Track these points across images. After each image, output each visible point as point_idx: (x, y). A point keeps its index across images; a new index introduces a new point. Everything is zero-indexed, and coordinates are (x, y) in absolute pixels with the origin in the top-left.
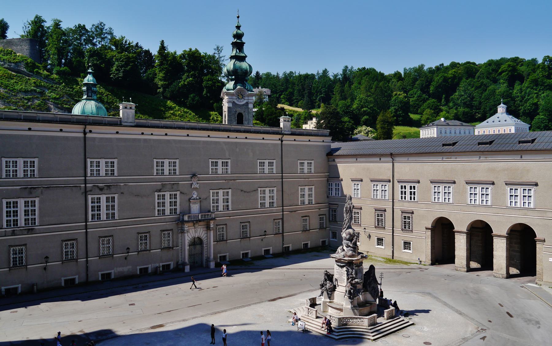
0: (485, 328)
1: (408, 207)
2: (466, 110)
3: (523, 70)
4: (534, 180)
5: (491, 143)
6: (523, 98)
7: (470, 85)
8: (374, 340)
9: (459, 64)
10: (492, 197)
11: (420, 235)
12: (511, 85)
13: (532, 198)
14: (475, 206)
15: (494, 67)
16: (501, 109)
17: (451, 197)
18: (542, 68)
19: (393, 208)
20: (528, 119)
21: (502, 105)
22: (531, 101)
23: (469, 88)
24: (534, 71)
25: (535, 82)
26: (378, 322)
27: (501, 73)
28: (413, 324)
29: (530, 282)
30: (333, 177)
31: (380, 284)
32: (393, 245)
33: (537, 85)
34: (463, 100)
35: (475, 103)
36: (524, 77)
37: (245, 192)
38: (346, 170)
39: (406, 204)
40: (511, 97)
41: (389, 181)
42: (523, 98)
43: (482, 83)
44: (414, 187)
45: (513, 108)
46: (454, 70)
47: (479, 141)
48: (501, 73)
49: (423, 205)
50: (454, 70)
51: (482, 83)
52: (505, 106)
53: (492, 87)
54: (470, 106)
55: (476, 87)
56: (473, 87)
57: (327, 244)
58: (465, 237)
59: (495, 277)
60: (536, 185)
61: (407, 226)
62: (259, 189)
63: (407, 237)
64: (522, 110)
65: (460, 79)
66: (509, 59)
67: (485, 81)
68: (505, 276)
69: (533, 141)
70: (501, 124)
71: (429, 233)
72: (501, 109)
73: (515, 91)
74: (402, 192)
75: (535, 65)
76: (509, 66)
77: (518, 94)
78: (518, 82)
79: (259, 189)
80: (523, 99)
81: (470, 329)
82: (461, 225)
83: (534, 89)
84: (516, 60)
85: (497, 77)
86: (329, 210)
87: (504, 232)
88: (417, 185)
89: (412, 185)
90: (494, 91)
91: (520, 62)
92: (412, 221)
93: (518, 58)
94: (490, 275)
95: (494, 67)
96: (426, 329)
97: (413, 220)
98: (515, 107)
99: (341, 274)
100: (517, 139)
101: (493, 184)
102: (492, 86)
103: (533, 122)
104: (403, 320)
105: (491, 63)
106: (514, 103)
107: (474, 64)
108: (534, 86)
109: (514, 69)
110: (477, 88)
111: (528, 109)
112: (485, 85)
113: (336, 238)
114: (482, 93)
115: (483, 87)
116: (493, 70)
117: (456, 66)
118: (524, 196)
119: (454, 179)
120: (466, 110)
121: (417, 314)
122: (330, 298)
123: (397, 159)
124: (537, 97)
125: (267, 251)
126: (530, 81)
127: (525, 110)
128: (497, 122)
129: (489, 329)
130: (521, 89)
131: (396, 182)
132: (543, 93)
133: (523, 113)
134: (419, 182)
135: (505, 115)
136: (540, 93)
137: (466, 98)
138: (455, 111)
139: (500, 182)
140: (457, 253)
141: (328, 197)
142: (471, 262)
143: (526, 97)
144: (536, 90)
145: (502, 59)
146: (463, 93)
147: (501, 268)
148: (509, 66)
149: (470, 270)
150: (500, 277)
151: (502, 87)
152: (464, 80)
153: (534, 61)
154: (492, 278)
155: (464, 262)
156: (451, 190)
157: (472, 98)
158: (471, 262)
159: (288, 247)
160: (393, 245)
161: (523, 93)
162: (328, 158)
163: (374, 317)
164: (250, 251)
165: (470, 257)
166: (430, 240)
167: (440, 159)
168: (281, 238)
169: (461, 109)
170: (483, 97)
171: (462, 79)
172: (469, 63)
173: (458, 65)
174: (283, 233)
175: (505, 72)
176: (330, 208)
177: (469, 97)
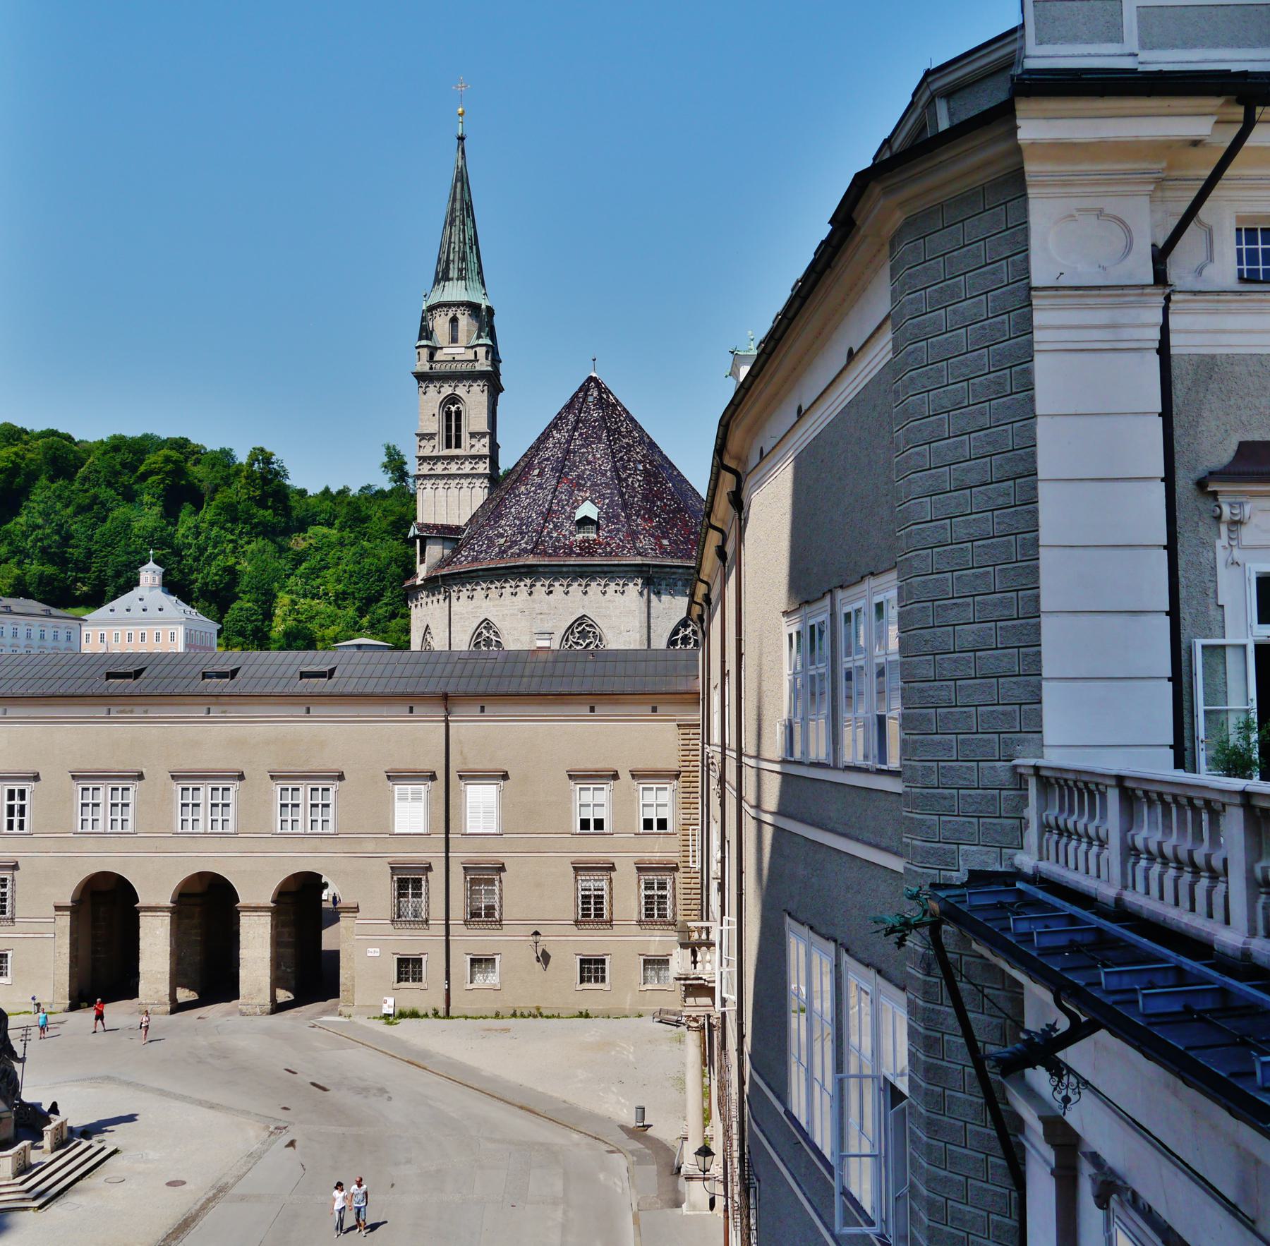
0: (282, 1124)
2: (49, 570)
3: (199, 476)
4: (335, 766)
5: (137, 674)
6: (201, 550)
7: (60, 497)
8: (40, 1207)
9: (24, 431)
11: (37, 928)
12: (171, 513)
13: (331, 809)
14: (193, 836)
15: (128, 457)
16: (150, 575)
17: (130, 817)
18: (247, 478)
20: (214, 607)
21: (151, 565)
22: (220, 561)
23: (59, 506)
24: (227, 481)
25: (231, 513)
26: (34, 1162)
27: (144, 477)
28: (115, 1152)
29: (325, 1012)
31: (22, 1060)
33: (234, 520)
34: (41, 540)
35: (75, 553)
36: (202, 496)
40: (170, 546)
42: (201, 550)
43: (95, 497)
44: (22, 794)
45: (176, 576)
46: (15, 449)
47: (105, 669)
48: (144, 477)
49: (49, 843)
50: (15, 449)
51: (95, 497)
52: (160, 570)
53: (121, 511)
54: (59, 559)
55: (79, 506)
56: (67, 506)
58: (167, 920)
59: (243, 1014)
60: (341, 777)
64: (198, 584)
65: (32, 477)
66: (165, 441)
67: (105, 493)
68: (268, 1007)
69: (233, 674)
70: (147, 621)
71: (65, 920)
72: (150, 575)
73: (181, 531)
74: (11, 808)
75: (228, 466)
76: (167, 460)
77: (190, 540)
78: (188, 507)
80: (202, 554)
81: (252, 1133)
82: (155, 889)
83: (226, 529)
84: (181, 444)
85: (136, 487)
87: (267, 899)
88: (29, 787)
89: (17, 787)
90: (127, 525)
91: (193, 453)
92: (13, 891)
93: (187, 440)
94: (229, 1014)
95: (128, 454)
96: (152, 1155)
97: (17, 888)
98: (181, 571)
100: (199, 668)
101: (241, 777)
102: (121, 509)
103: (227, 617)
104: (90, 1147)
105: (117, 445)
106: (179, 563)
107: (69, 438)
108: (227, 521)
109: (178, 471)
110: (81, 510)
111: (215, 582)
112: (103, 504)
114: (93, 527)
115: (95, 509)
116: (124, 465)
117: (19, 439)
118: (312, 806)
119: (139, 768)
120: (49, 570)
121: (109, 1128)
124: (233, 552)
126: (217, 507)
127: (206, 584)
128: (137, 613)
129: (290, 1123)
130: (196, 527)
132: (249, 543)
133: (200, 590)
134: (36, 778)
135: (159, 592)
136: (240, 542)
137: (47, 537)
138: (17, 571)
140: (143, 966)
142: (179, 990)
143: (210, 550)
144: (232, 532)
145: (146, 437)
146: (40, 521)
147: (260, 990)
149: (177, 1007)
150: (255, 1014)
151: (147, 517)
152: (43, 481)
153: (226, 454)
154: (237, 1018)
155: (165, 989)
156: (131, 797)
157: (67, 538)
158: (179, 990)
161: (202, 538)
163: (25, 1149)
165: (178, 978)
166: (67, 941)
167: (101, 712)
169: (35, 568)
170: (96, 537)
171: (37, 479)
172: (53, 433)
173: (25, 437)
175: (158, 474)
177: (58, 532)
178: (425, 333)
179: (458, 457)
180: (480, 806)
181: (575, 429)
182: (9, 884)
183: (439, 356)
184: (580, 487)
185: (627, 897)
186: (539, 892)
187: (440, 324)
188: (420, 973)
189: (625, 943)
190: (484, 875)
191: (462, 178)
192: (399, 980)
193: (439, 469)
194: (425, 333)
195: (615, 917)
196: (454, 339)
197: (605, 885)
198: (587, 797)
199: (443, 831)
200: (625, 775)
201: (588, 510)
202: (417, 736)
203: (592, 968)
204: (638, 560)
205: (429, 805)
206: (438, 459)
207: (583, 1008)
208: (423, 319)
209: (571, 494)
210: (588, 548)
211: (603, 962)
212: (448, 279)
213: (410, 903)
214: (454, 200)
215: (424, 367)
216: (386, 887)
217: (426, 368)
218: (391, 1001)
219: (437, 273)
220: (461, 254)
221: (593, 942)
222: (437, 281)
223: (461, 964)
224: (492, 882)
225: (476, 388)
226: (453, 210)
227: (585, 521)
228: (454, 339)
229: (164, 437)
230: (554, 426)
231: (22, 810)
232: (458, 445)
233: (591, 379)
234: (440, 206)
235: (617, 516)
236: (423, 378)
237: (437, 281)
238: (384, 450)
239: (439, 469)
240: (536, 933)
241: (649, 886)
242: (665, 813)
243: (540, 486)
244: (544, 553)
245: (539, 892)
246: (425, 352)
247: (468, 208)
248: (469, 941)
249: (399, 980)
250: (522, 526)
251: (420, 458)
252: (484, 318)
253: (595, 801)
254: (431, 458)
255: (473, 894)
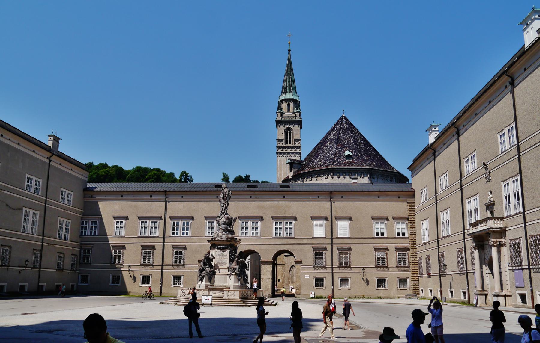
1: (179, 242)
10: (261, 230)
19: (164, 245)
30: (90, 213)
32: (162, 281)
37: (10, 208)
38: (108, 209)
39: (178, 240)
41: (160, 218)
57: (75, 289)
61: (178, 262)
62: (24, 209)
63: (178, 272)
79: (24, 209)
86: (80, 251)
99: (223, 257)
113: (87, 283)
122: (210, 282)
123: (171, 197)
125: (23, 287)
131: (168, 218)
139: (267, 217)
141: (80, 237)
147: (268, 289)
148: (155, 174)
159: (42, 286)
160: (162, 281)
162: (84, 194)
164: (6, 284)
168: (37, 273)
174: (40, 268)
176: (81, 249)
178: (280, 108)
179: (290, 147)
180: (343, 228)
181: (340, 130)
182: (151, 253)
183: (284, 115)
184: (345, 147)
185: (393, 259)
186: (363, 256)
187: (284, 106)
188: (323, 284)
189: (392, 275)
190: (344, 251)
191: (290, 62)
192: (316, 286)
193: (284, 151)
194: (280, 108)
195: (389, 264)
196: (289, 110)
197: (385, 255)
198: (378, 226)
199: (165, 246)
200: (391, 219)
201: (347, 153)
202: (322, 207)
203: (381, 282)
204: (368, 167)
205: (326, 228)
206: (284, 147)
207: (379, 295)
208: (279, 104)
209: (342, 149)
210: (350, 164)
211: (385, 280)
212: (287, 92)
213: (319, 262)
214: (288, 68)
215: (279, 118)
216: (312, 254)
217: (280, 119)
218: (313, 293)
219: (282, 91)
220: (290, 85)
221: (382, 274)
222: (282, 93)
223: (337, 281)
224: (347, 254)
225: (296, 126)
226: (287, 72)
227: (349, 156)
228: (289, 110)
229: (152, 168)
230: (333, 129)
231: (187, 228)
232: (290, 143)
233: (343, 116)
234: (284, 71)
235: (358, 155)
236: (278, 123)
237: (282, 93)
238: (222, 175)
239: (284, 151)
240: (364, 269)
241: (400, 255)
242: (404, 231)
243: (331, 147)
244: (337, 165)
245: (363, 256)
246: (279, 114)
247: (292, 71)
248: (339, 274)
249: (316, 286)
250: (327, 158)
251: (278, 147)
252: (297, 104)
253: (381, 227)
254: (282, 147)
255: (340, 258)
